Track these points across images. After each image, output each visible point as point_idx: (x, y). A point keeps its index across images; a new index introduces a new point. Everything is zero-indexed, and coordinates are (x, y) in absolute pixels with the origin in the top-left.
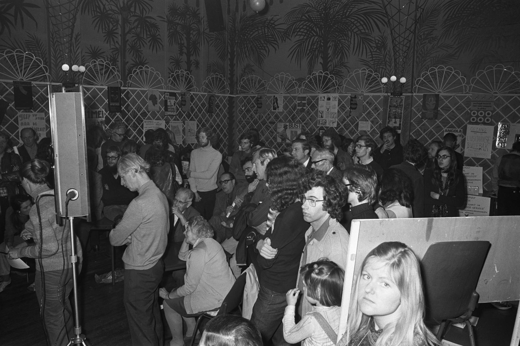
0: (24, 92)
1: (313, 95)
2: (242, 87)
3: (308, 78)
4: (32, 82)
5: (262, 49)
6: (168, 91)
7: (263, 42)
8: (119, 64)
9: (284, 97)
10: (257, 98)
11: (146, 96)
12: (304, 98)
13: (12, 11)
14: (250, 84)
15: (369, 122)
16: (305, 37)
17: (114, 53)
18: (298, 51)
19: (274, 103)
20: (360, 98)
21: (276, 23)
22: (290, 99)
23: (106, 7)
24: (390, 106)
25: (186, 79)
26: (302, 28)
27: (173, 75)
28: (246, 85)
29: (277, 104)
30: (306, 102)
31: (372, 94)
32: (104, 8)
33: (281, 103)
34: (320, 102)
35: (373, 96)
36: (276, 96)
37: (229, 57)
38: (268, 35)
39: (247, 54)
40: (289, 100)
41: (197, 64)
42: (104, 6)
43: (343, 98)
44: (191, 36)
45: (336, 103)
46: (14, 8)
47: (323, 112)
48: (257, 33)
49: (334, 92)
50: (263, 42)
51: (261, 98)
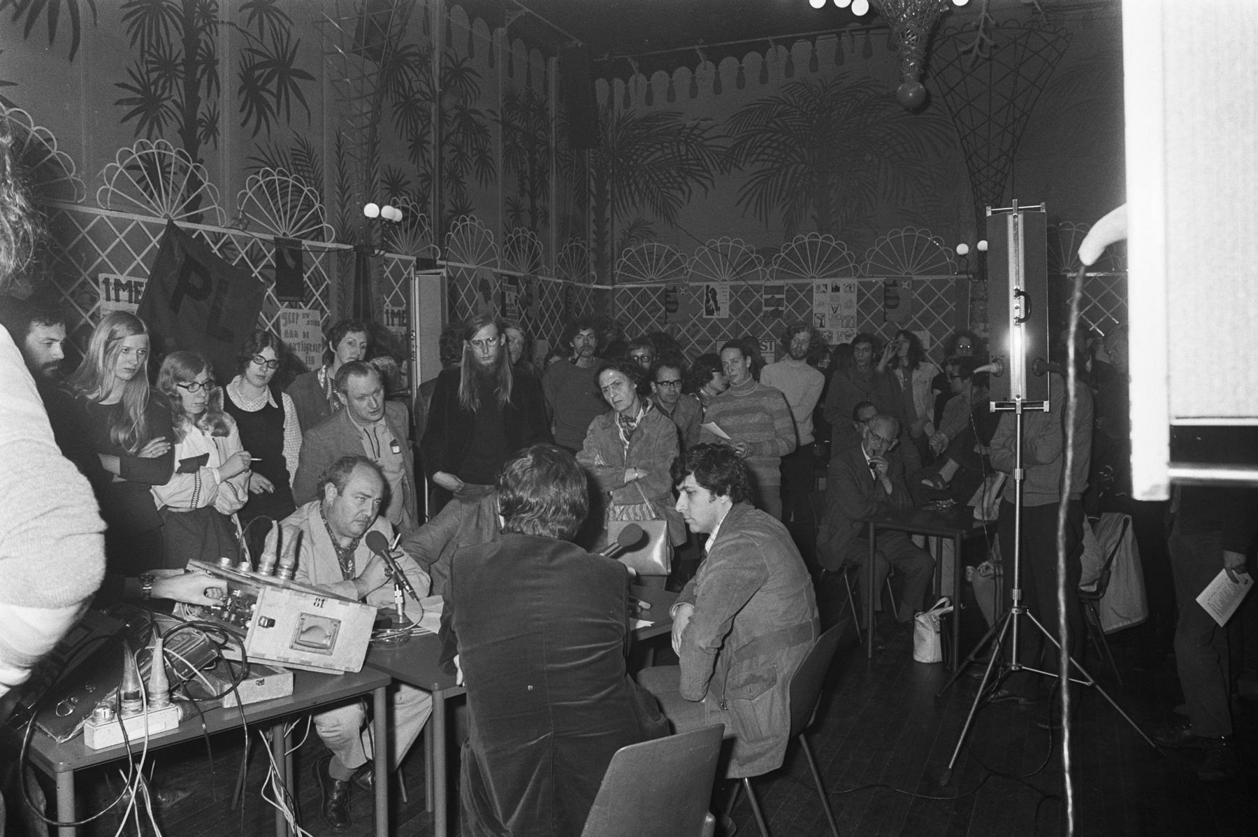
0: (290, 262)
1: (800, 281)
2: (626, 268)
3: (786, 248)
4: (304, 242)
5: (673, 188)
6: (506, 272)
7: (674, 173)
8: (431, 208)
9: (731, 287)
10: (666, 290)
11: (474, 282)
12: (779, 289)
13: (273, 86)
14: (644, 262)
15: (927, 332)
16: (777, 165)
17: (425, 184)
18: (761, 194)
19: (708, 301)
20: (905, 285)
21: (706, 135)
22: (747, 291)
23: (414, 84)
24: (973, 300)
25: (530, 249)
26: (768, 146)
27: (511, 238)
28: (637, 264)
29: (716, 302)
30: (784, 296)
31: (930, 278)
32: (410, 87)
33: (724, 300)
34: (817, 297)
35: (933, 282)
36: (712, 285)
37: (593, 202)
38: (688, 159)
39: (637, 199)
40: (741, 297)
41: (546, 215)
42: (410, 82)
43: (869, 286)
44: (537, 156)
45: (854, 297)
46: (276, 79)
47: (823, 316)
48: (659, 154)
49: (846, 274)
50: (674, 173)
51: (674, 290)
